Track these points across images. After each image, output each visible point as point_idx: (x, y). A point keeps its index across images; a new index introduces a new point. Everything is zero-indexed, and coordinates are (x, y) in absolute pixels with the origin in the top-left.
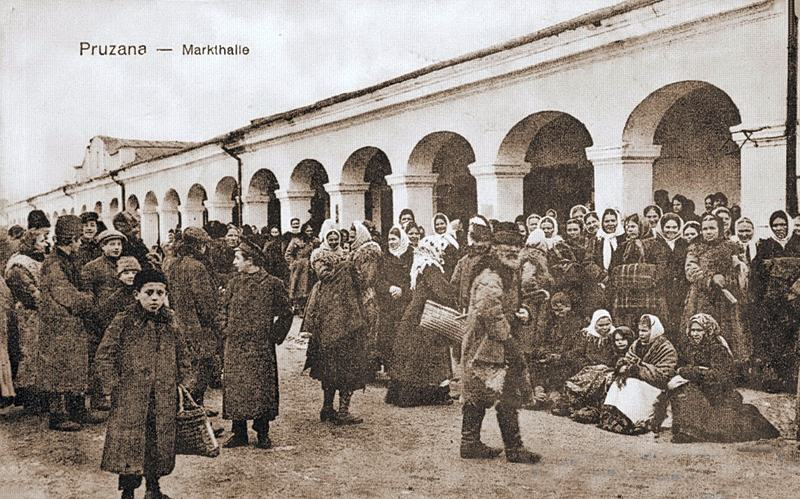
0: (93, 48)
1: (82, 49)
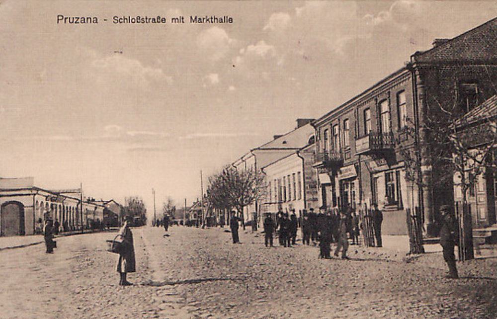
0: (66, 19)
1: (58, 20)
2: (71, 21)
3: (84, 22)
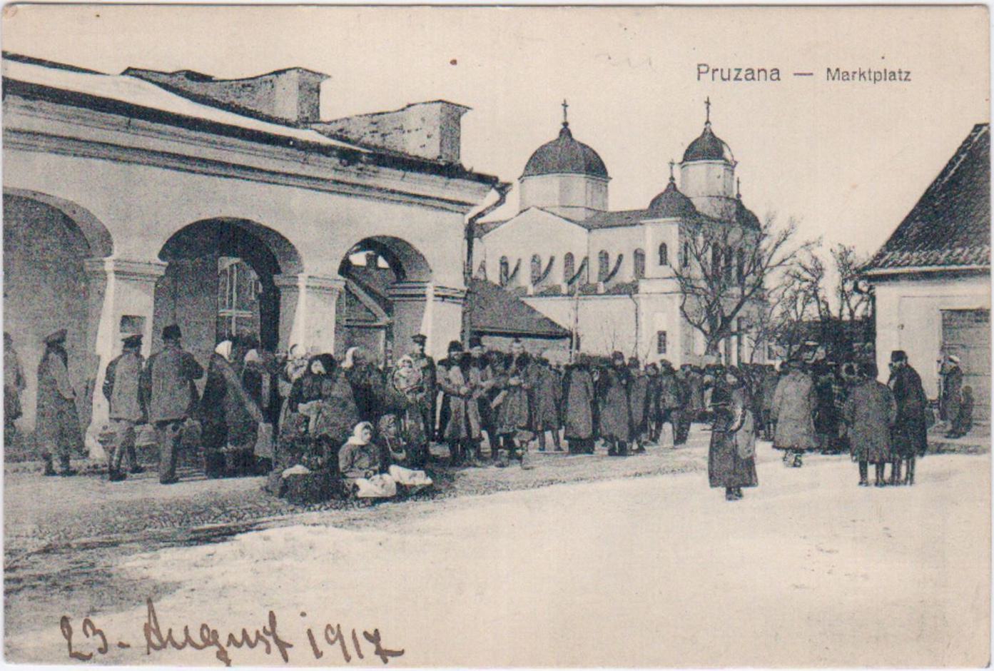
1: (699, 73)
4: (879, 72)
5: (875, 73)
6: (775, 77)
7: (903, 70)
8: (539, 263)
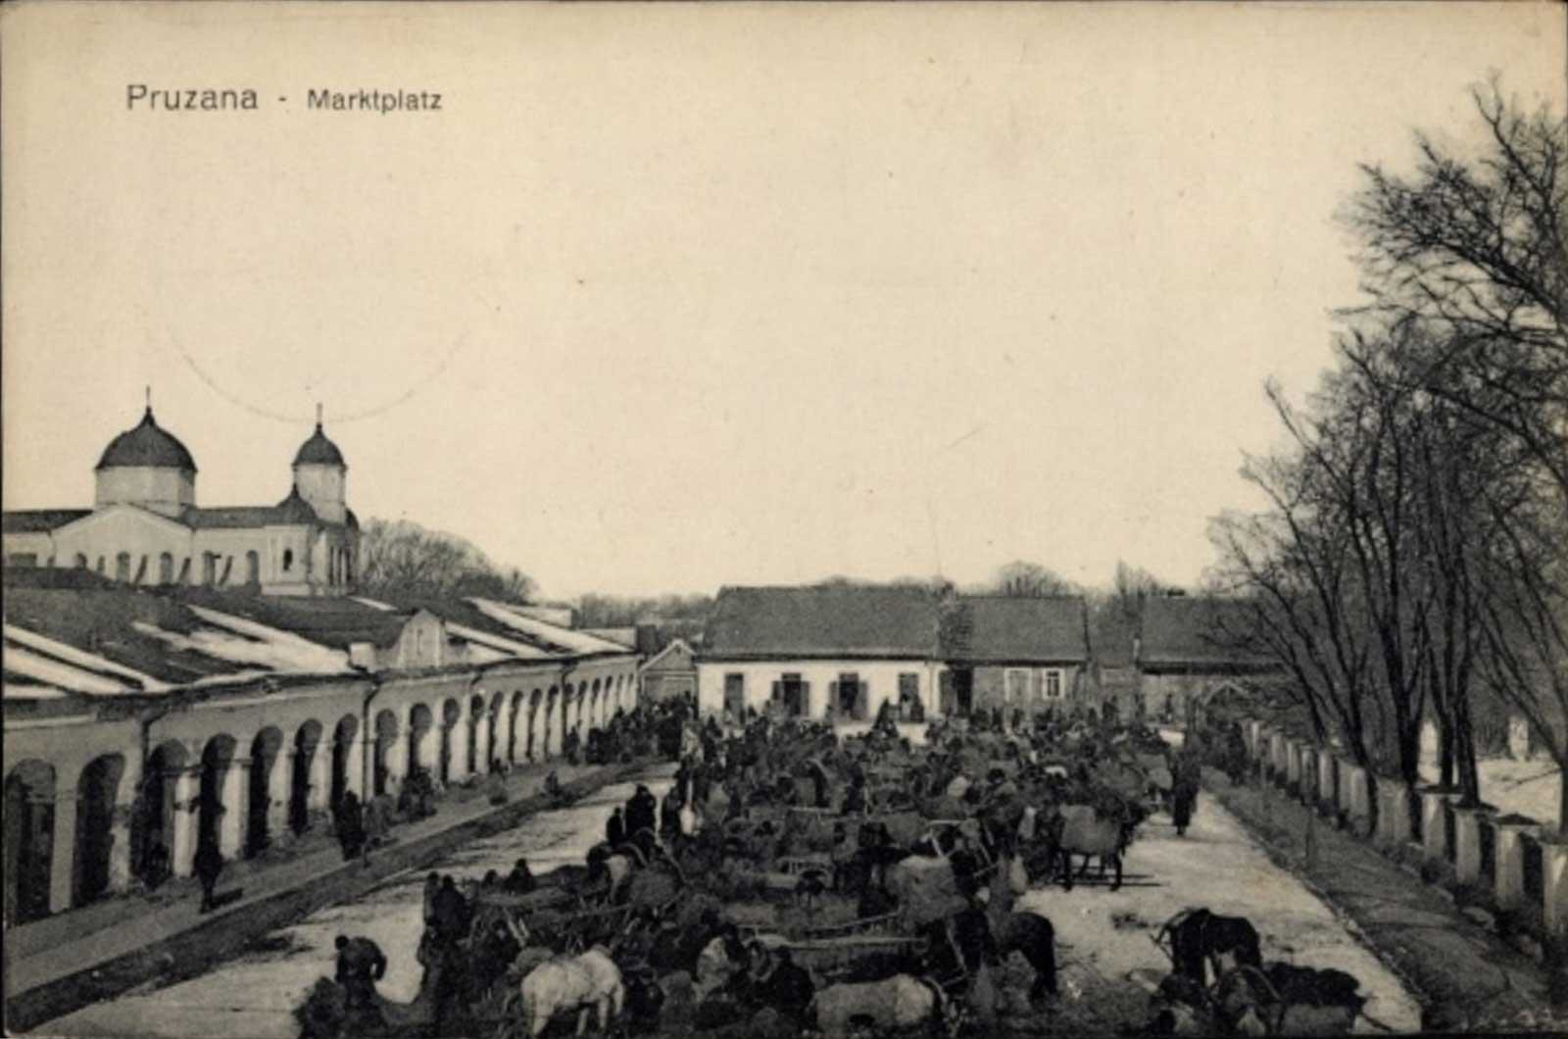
0: (153, 95)
1: (132, 97)
2: (172, 102)
3: (343, 107)
4: (391, 96)
5: (384, 98)
6: (249, 103)
7: (429, 93)
8: (127, 565)
